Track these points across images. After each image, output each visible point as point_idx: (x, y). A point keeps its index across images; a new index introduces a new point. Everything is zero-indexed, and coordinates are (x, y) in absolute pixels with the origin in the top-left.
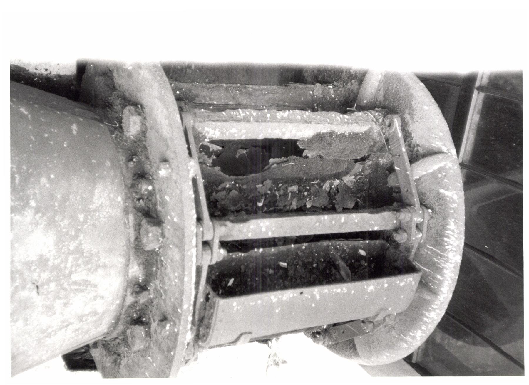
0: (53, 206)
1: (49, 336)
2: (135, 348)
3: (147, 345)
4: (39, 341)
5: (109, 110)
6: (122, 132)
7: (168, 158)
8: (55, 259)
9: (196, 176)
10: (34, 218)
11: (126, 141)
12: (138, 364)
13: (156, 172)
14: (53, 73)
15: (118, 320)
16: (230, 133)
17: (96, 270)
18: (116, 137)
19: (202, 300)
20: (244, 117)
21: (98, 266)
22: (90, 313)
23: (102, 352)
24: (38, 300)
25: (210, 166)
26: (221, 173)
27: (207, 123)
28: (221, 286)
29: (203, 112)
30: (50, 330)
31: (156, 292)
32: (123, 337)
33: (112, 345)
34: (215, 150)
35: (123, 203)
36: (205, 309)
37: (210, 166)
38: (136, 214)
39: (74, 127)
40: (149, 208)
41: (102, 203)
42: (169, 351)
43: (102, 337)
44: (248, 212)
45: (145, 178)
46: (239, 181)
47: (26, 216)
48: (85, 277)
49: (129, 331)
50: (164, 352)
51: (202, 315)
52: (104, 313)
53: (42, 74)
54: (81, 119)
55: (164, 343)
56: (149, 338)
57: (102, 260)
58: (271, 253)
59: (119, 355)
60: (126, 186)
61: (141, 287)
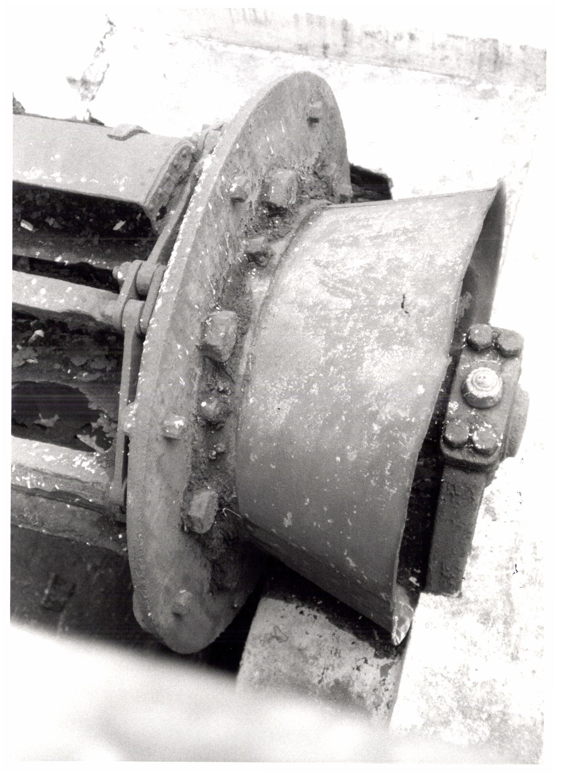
0: (347, 416)
1: (405, 231)
2: (290, 173)
3: (271, 172)
4: (420, 229)
5: (231, 534)
6: (221, 498)
7: (165, 442)
8: (368, 338)
9: (128, 403)
10: (380, 408)
11: (219, 483)
12: (291, 146)
13: (188, 426)
14: (294, 606)
15: (304, 224)
16: (56, 456)
17: (316, 305)
18: (232, 493)
19: (172, 212)
20: (26, 475)
21: (309, 308)
22: (341, 246)
23: (336, 185)
24: (407, 288)
25: (103, 413)
26: (89, 397)
27: (88, 480)
28: (135, 225)
29: (91, 497)
30: (403, 238)
31: (237, 246)
32: (304, 196)
33: (321, 190)
34: (88, 436)
35: (247, 393)
36: (171, 197)
37: (103, 413)
38: (234, 372)
39: (287, 522)
40: (213, 376)
41: (279, 402)
42: (241, 152)
43: (330, 206)
44: (63, 326)
45: (206, 420)
46: (63, 377)
47: (389, 413)
48: (335, 299)
49: (293, 201)
50: (249, 153)
51: (179, 189)
52: (317, 241)
53: (309, 608)
54: (274, 530)
55: (246, 166)
56: (266, 181)
57: (302, 316)
58: (43, 250)
59: (315, 173)
60: (237, 416)
61: (255, 260)
